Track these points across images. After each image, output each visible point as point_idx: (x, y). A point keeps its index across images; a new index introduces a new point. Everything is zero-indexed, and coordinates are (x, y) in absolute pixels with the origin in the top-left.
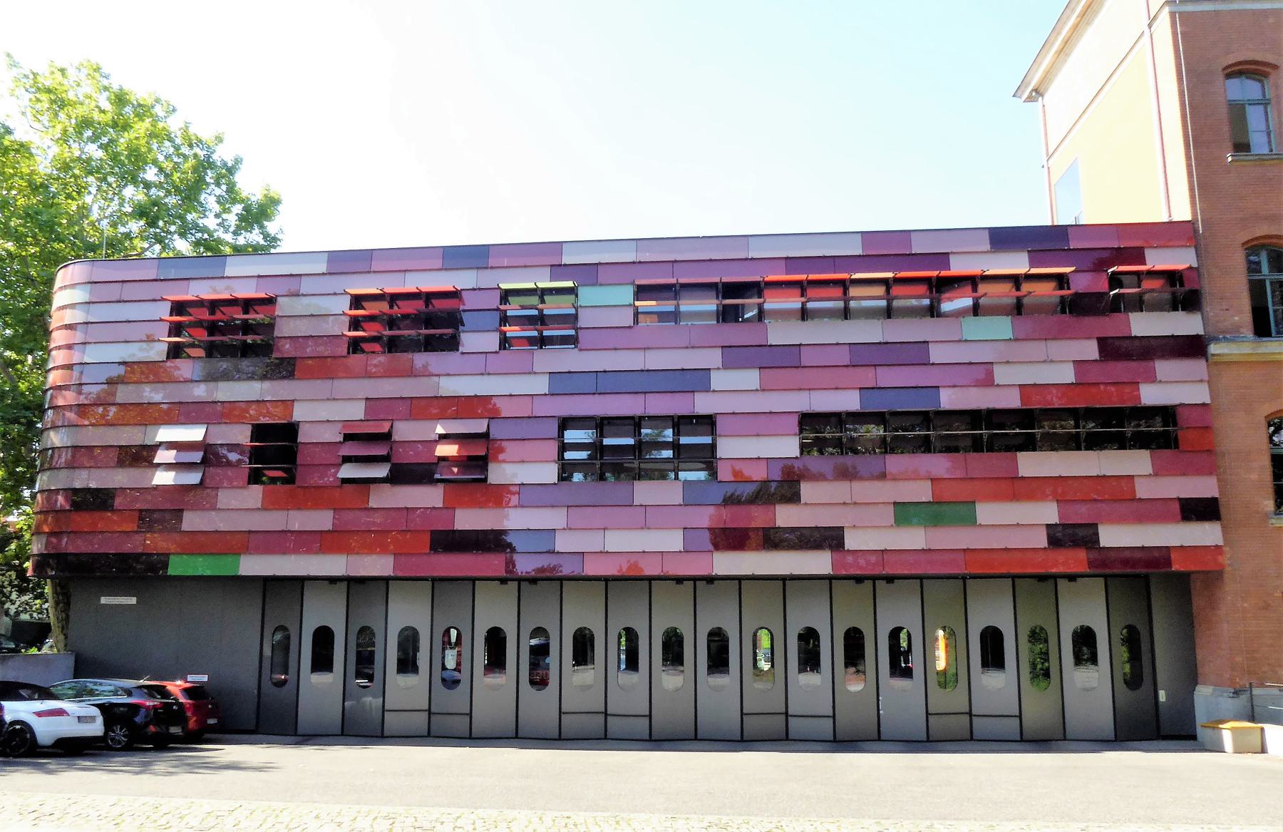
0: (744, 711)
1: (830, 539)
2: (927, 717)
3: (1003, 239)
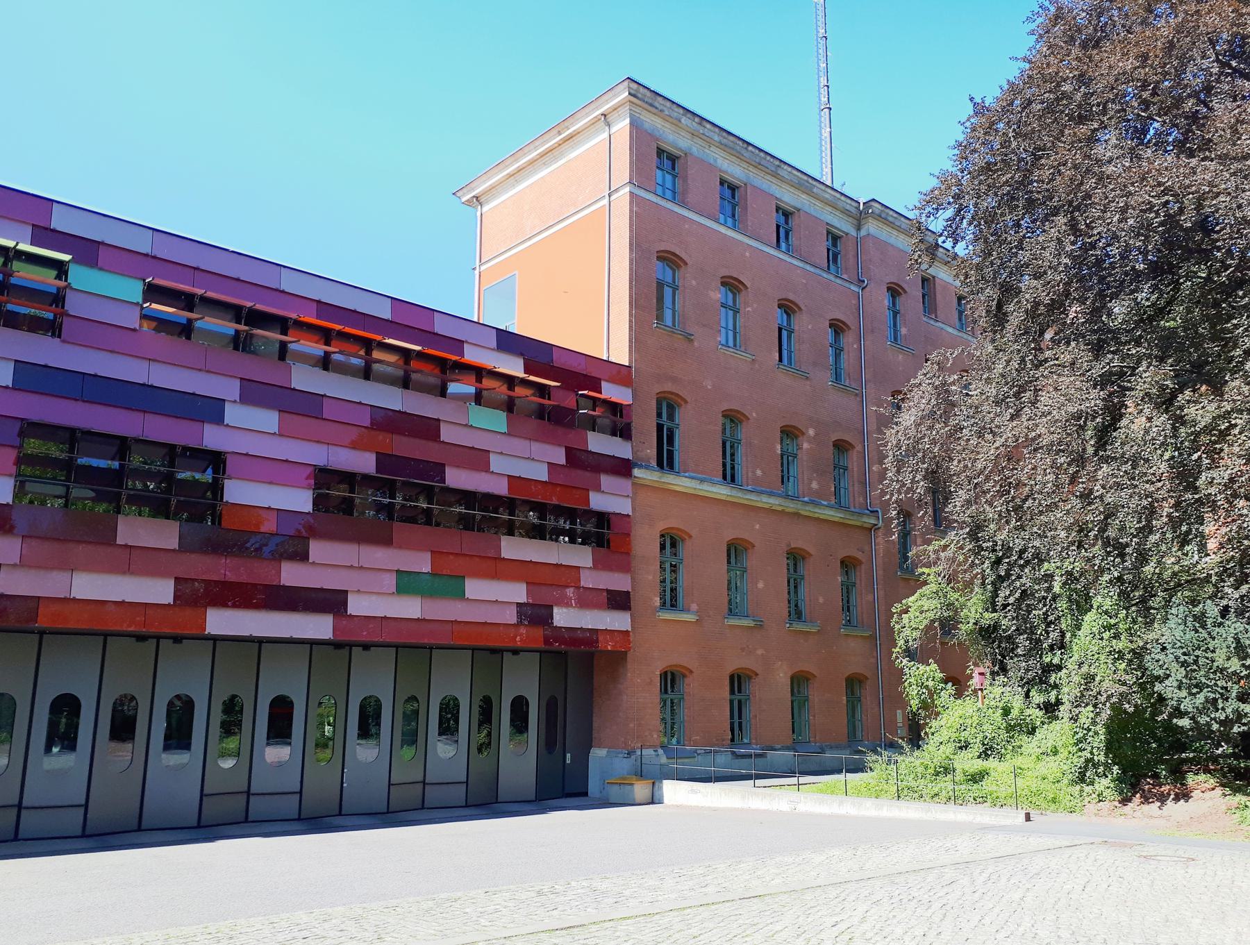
1: (332, 602)
2: (201, 800)
3: (508, 341)
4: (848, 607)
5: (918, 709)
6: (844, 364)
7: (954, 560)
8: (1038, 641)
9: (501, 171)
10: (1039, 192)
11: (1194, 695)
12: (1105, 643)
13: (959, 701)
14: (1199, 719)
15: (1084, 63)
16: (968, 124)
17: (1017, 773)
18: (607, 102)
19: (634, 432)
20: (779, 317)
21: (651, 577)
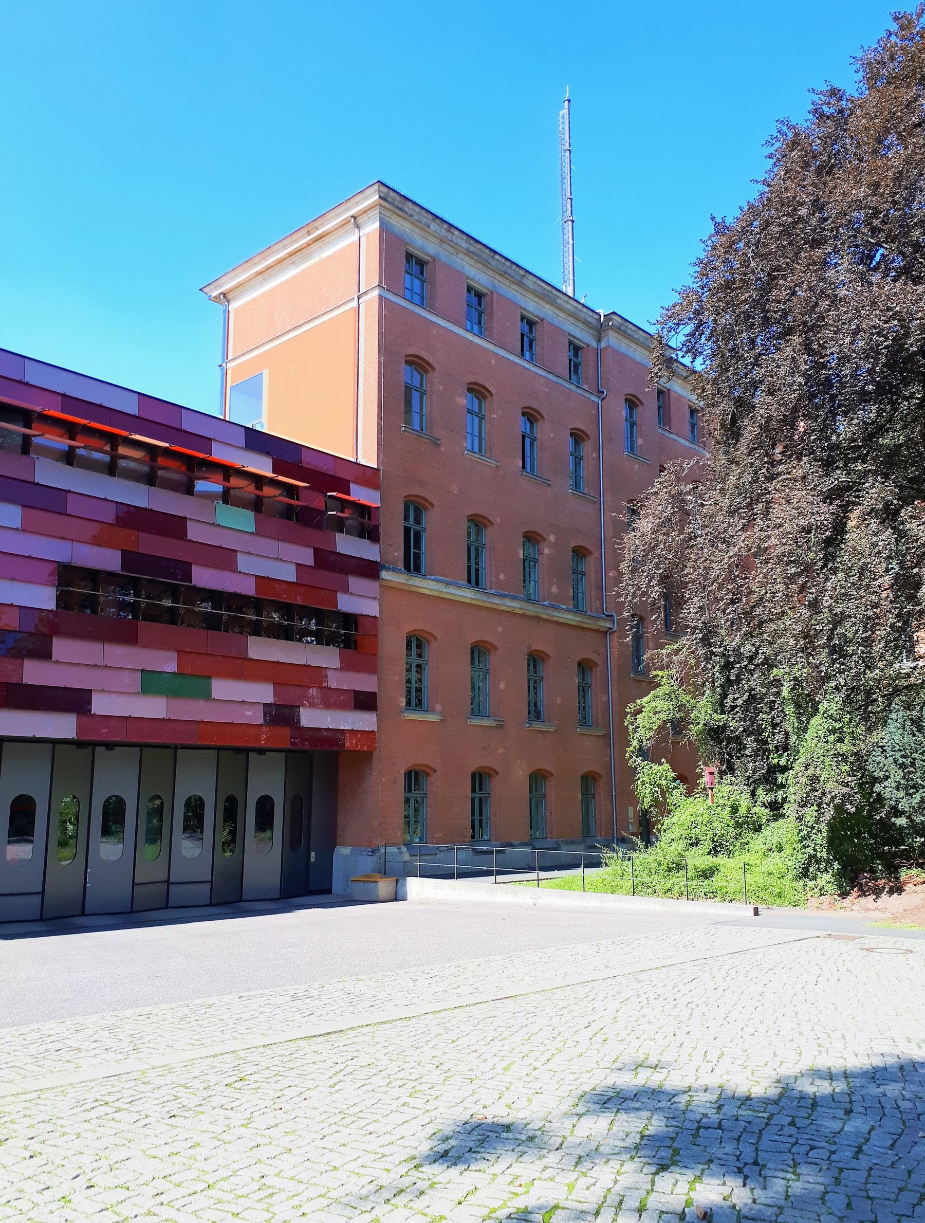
0: (135, 882)
4: (584, 707)
5: (650, 807)
6: (583, 473)
7: (686, 663)
8: (765, 742)
9: (249, 269)
10: (776, 312)
11: (911, 795)
12: (829, 746)
13: (691, 800)
14: (915, 818)
15: (820, 189)
16: (709, 243)
17: (746, 868)
18: (357, 204)
19: (382, 534)
20: (521, 425)
21: (397, 678)
